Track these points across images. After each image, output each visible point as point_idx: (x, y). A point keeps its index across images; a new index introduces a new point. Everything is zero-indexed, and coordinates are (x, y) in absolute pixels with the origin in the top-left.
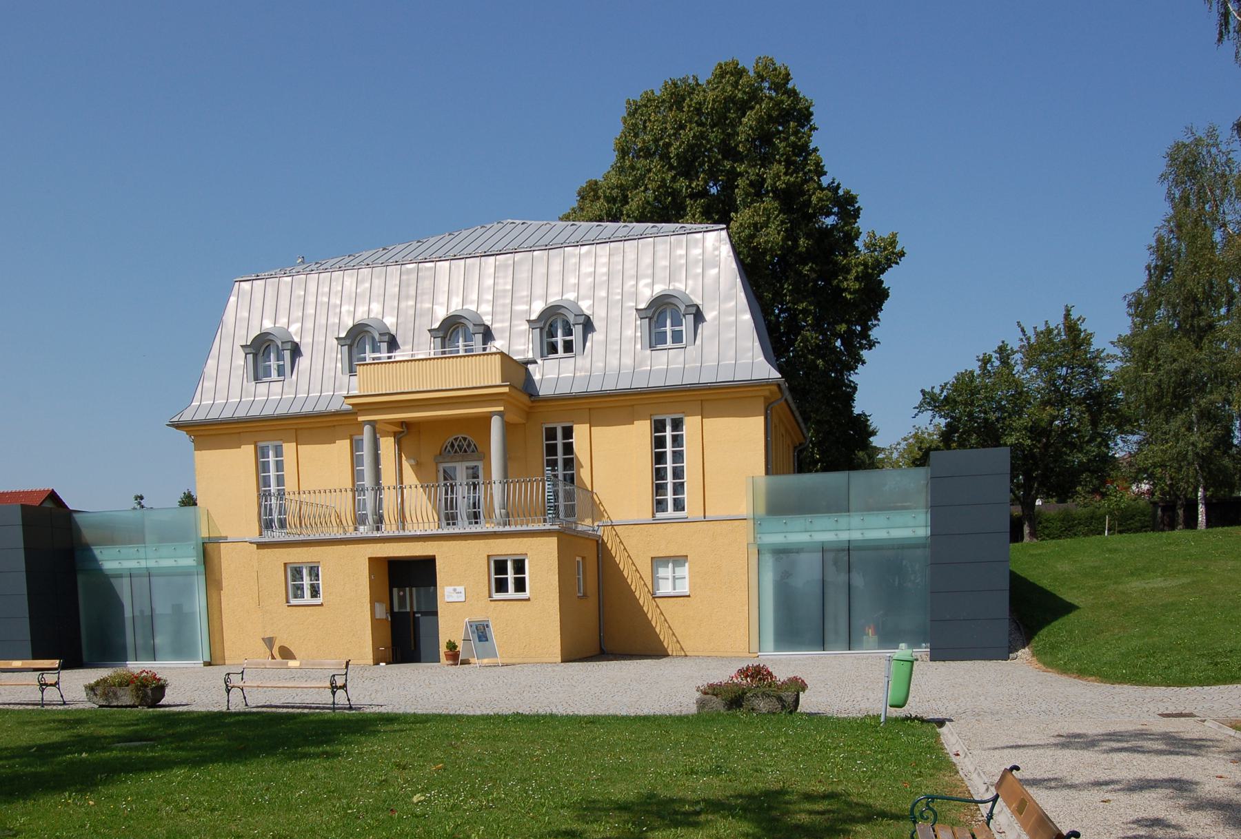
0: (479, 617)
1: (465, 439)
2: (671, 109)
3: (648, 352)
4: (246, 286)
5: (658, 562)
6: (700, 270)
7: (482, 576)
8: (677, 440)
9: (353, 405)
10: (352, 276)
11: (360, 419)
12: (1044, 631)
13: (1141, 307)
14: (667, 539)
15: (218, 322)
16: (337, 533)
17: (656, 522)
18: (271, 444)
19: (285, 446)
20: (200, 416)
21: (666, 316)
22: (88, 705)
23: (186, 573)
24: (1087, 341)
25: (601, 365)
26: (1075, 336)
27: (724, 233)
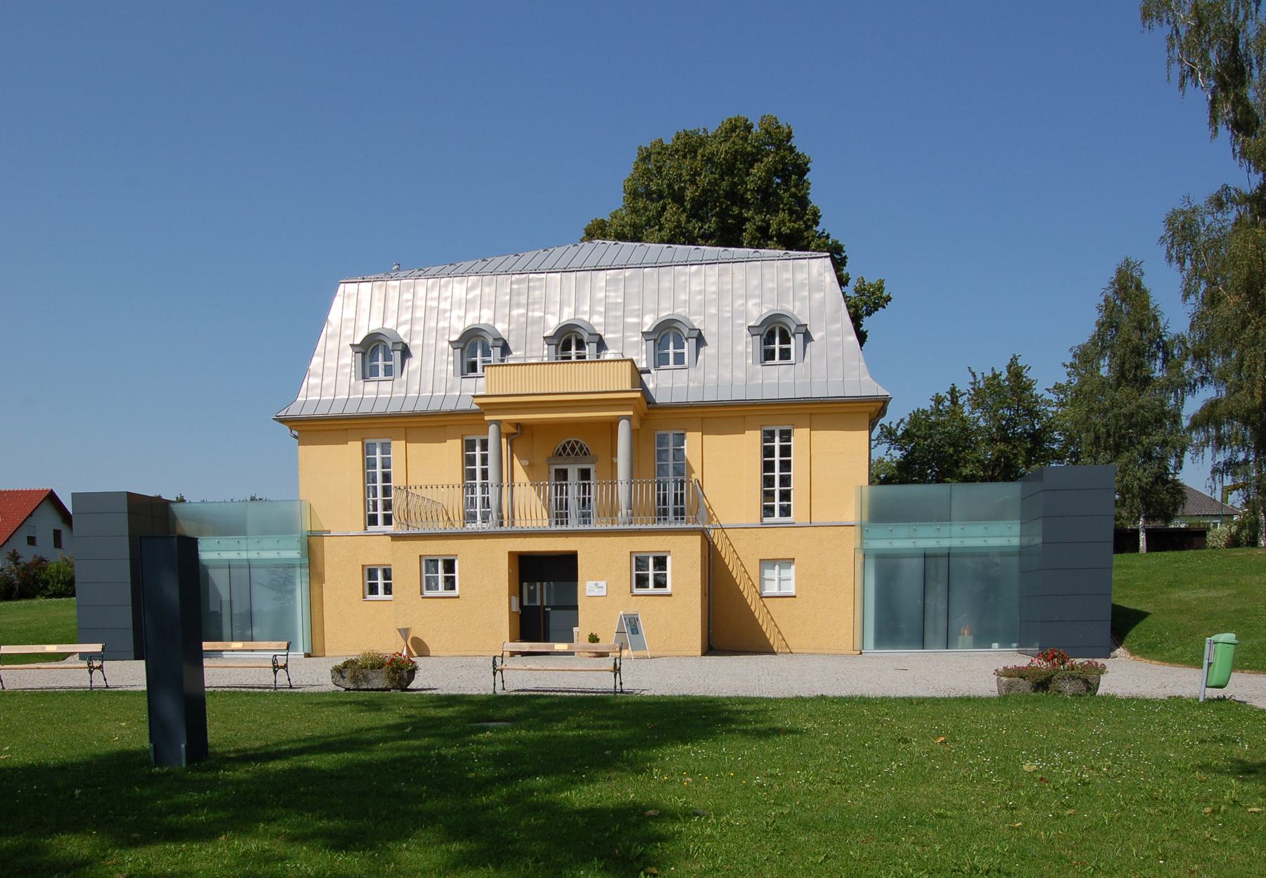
0: (631, 611)
1: (577, 442)
2: (685, 157)
3: (759, 367)
4: (351, 288)
5: (766, 563)
6: (806, 294)
7: (625, 573)
8: (786, 451)
9: (480, 404)
10: (380, 287)
11: (487, 418)
12: (1133, 632)
13: (1084, 358)
14: (776, 541)
15: (322, 319)
16: (440, 527)
17: (764, 526)
18: (378, 441)
19: (394, 443)
20: (307, 412)
21: (775, 336)
22: (332, 687)
23: (289, 566)
24: (1028, 387)
25: (714, 377)
26: (1017, 380)
27: (828, 261)
